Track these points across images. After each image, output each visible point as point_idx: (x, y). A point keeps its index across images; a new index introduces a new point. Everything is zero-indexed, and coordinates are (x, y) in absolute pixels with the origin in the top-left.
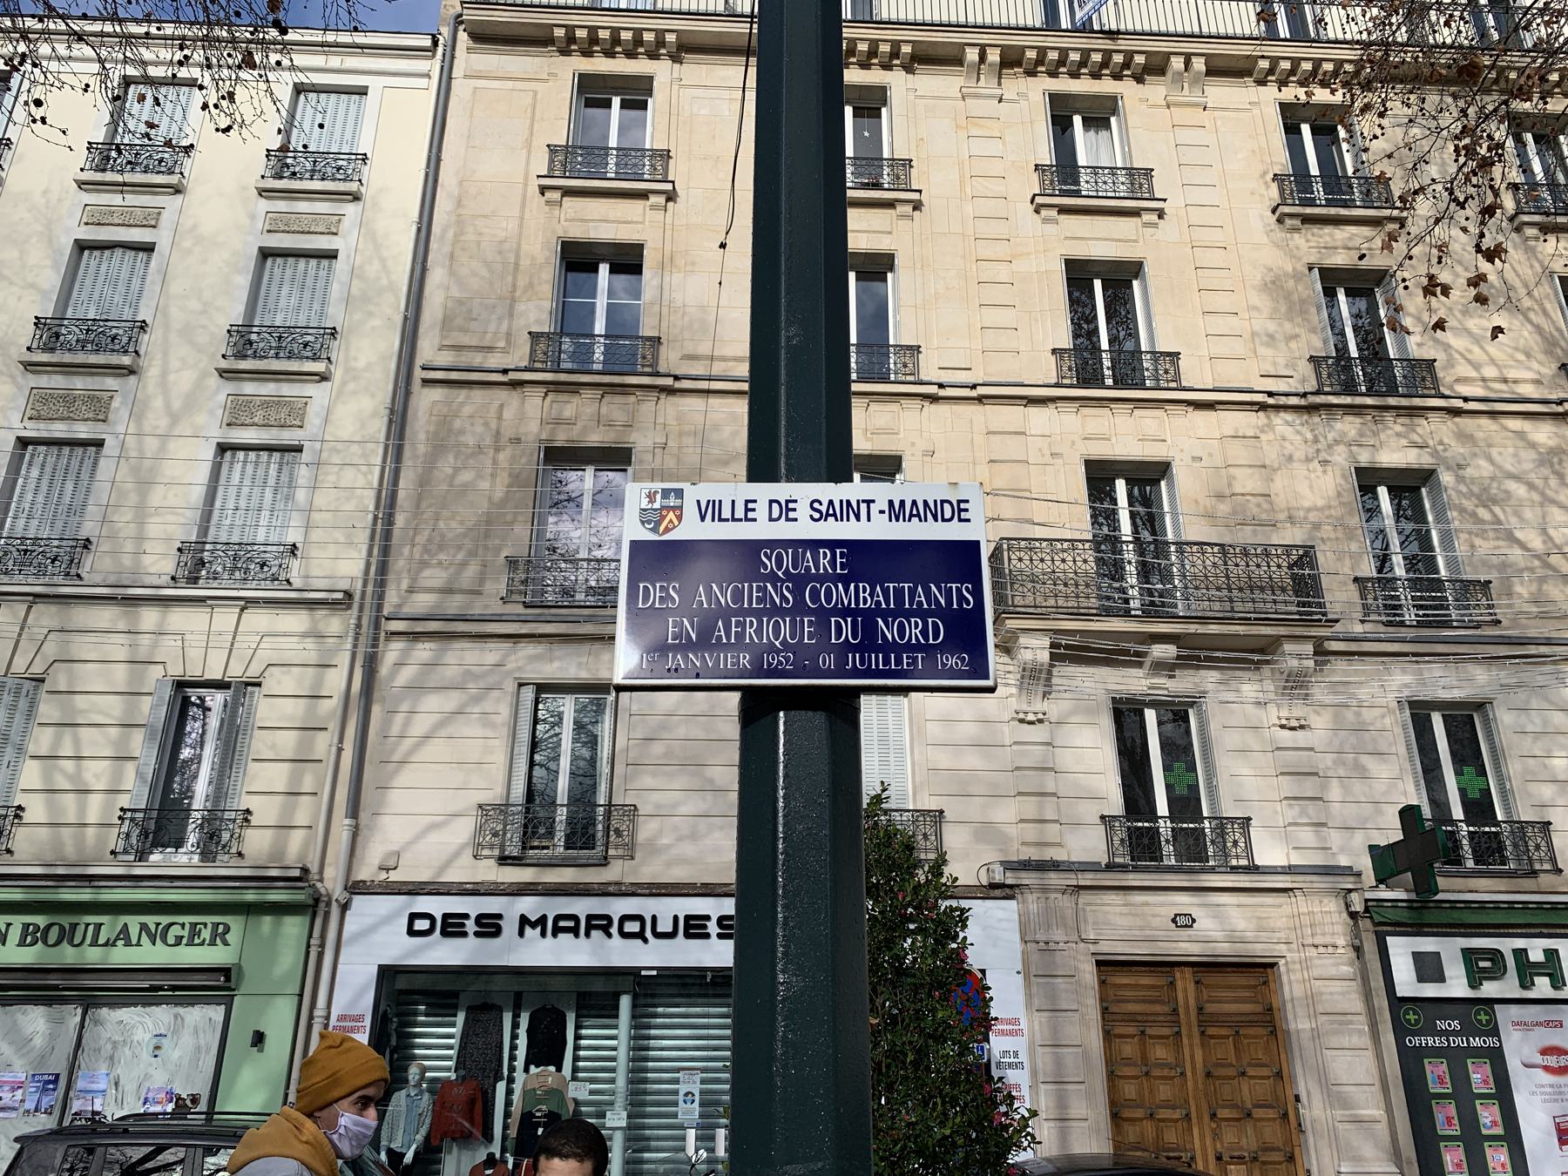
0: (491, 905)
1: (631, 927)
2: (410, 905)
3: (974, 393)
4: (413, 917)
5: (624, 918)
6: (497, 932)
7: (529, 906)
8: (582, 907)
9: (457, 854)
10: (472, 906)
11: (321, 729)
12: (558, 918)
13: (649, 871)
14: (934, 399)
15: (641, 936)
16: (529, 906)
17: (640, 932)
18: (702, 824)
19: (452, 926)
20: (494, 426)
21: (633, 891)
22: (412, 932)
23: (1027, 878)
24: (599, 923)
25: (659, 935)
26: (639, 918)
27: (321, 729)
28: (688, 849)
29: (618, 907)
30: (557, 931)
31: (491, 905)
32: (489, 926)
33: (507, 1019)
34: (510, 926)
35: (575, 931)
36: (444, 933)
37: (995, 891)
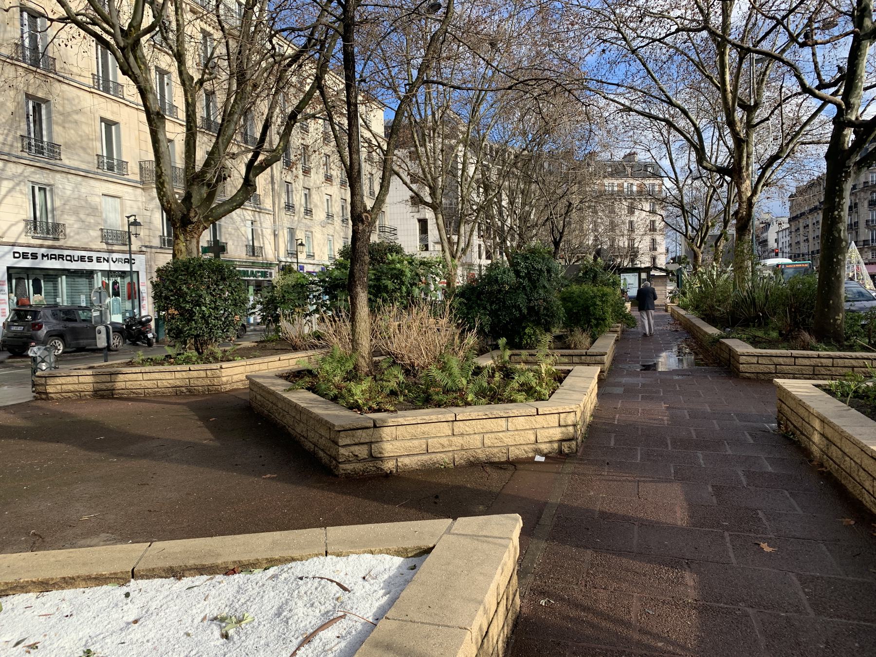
0: (99, 254)
1: (69, 258)
2: (12, 249)
3: (136, 107)
4: (14, 253)
5: (67, 256)
6: (37, 258)
7: (43, 251)
8: (57, 252)
9: (20, 234)
10: (30, 251)
11: (105, 195)
12: (51, 255)
13: (70, 243)
14: (127, 105)
15: (71, 260)
16: (43, 251)
17: (71, 259)
18: (80, 230)
19: (25, 256)
20: (280, 97)
21: (67, 248)
22: (15, 257)
23: (149, 250)
24: (61, 257)
25: (75, 261)
26: (70, 256)
27: (105, 195)
28: (77, 237)
29: (66, 253)
30: (51, 258)
31: (35, 250)
32: (34, 256)
33: (26, 281)
34: (40, 257)
35: (55, 258)
36: (23, 258)
37: (141, 252)
